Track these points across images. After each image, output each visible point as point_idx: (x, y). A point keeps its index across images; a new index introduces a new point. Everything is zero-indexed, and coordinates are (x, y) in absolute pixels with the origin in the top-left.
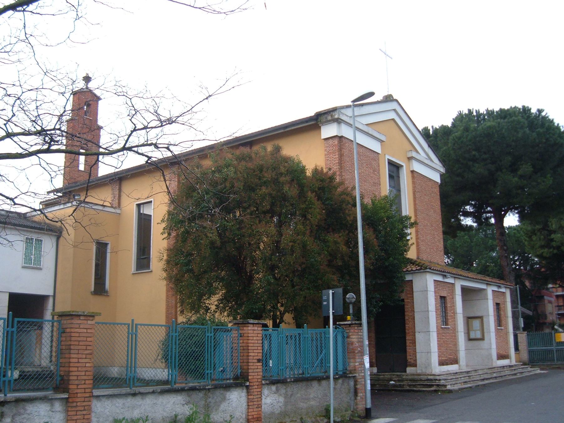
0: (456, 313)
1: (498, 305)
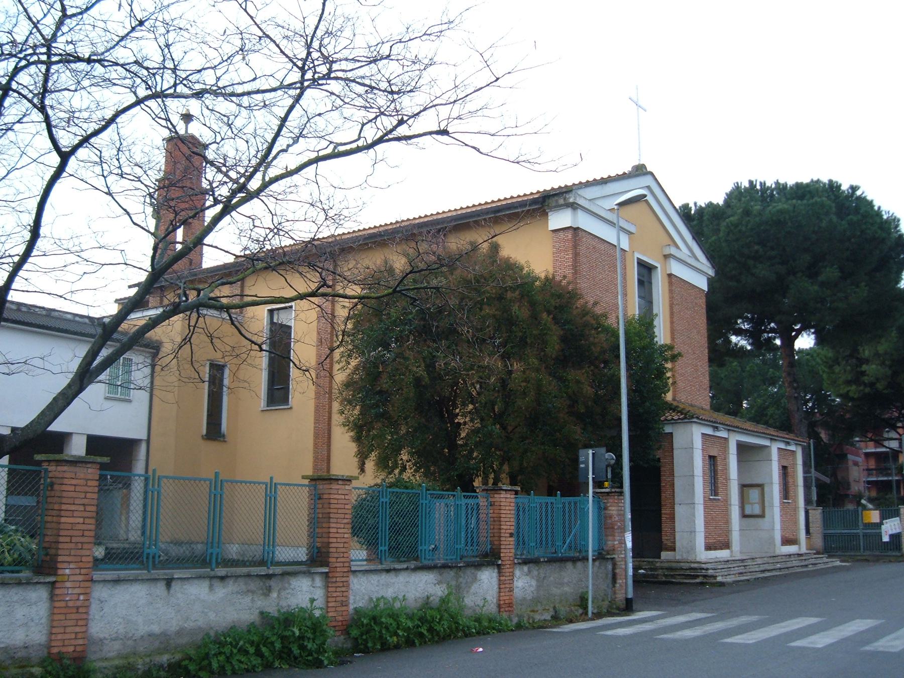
1: (784, 468)
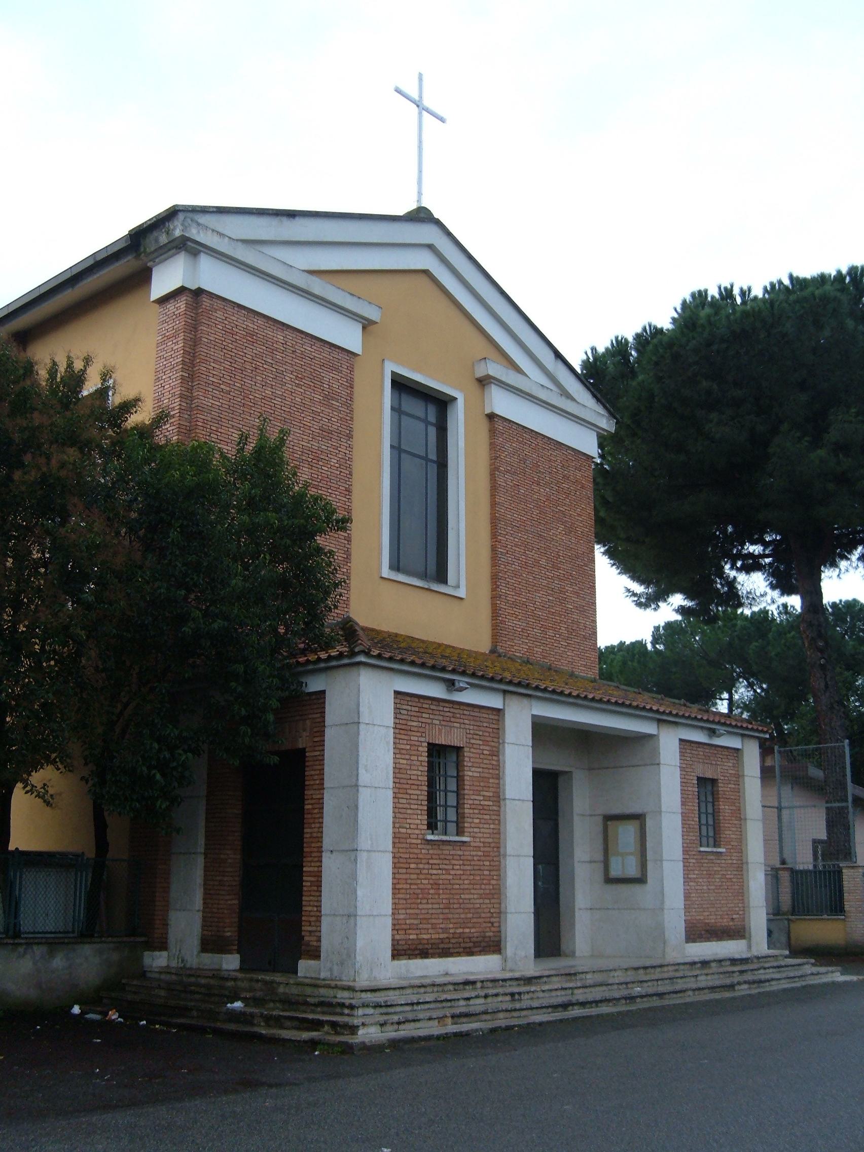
0: (505, 799)
